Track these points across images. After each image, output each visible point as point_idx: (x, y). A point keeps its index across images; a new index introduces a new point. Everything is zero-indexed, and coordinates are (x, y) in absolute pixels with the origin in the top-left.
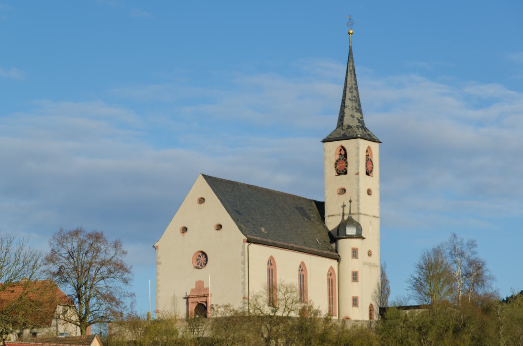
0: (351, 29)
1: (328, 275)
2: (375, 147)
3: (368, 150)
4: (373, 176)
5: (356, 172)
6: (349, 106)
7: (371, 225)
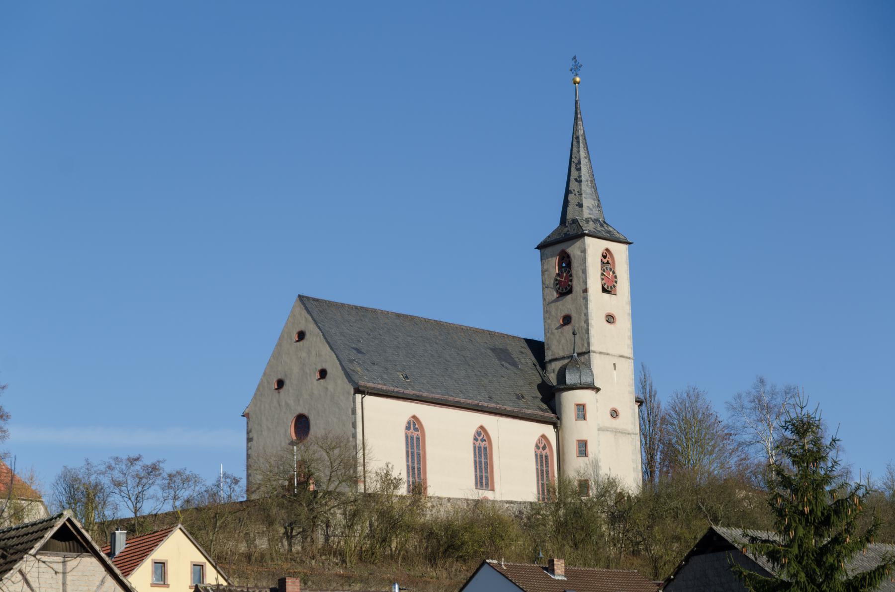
0: (577, 75)
1: (537, 446)
2: (620, 251)
3: (607, 255)
4: (618, 293)
5: (584, 288)
6: (576, 190)
7: (615, 369)
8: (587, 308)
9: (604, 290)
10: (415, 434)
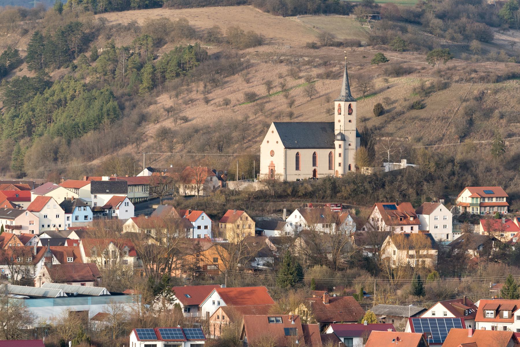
9: (349, 114)
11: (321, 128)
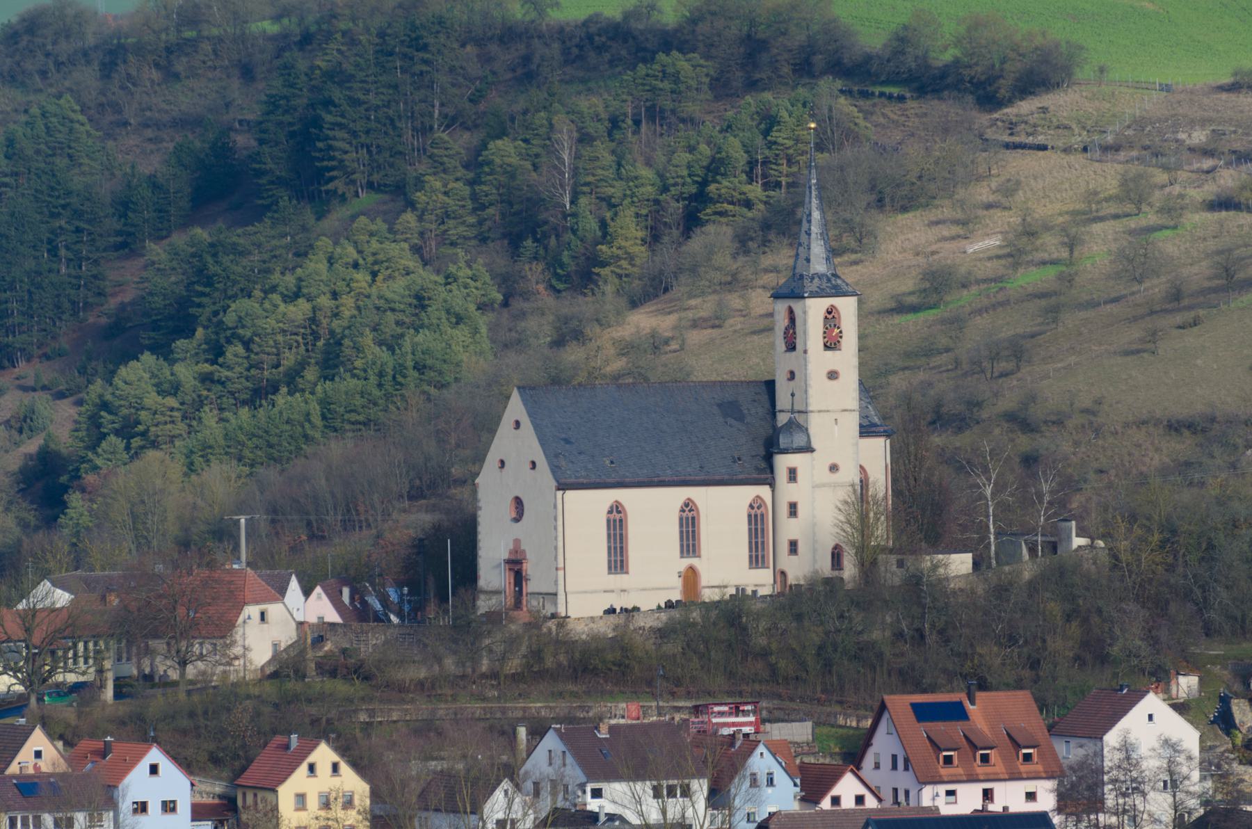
8: (806, 369)
9: (827, 347)
10: (618, 516)
11: (719, 405)
